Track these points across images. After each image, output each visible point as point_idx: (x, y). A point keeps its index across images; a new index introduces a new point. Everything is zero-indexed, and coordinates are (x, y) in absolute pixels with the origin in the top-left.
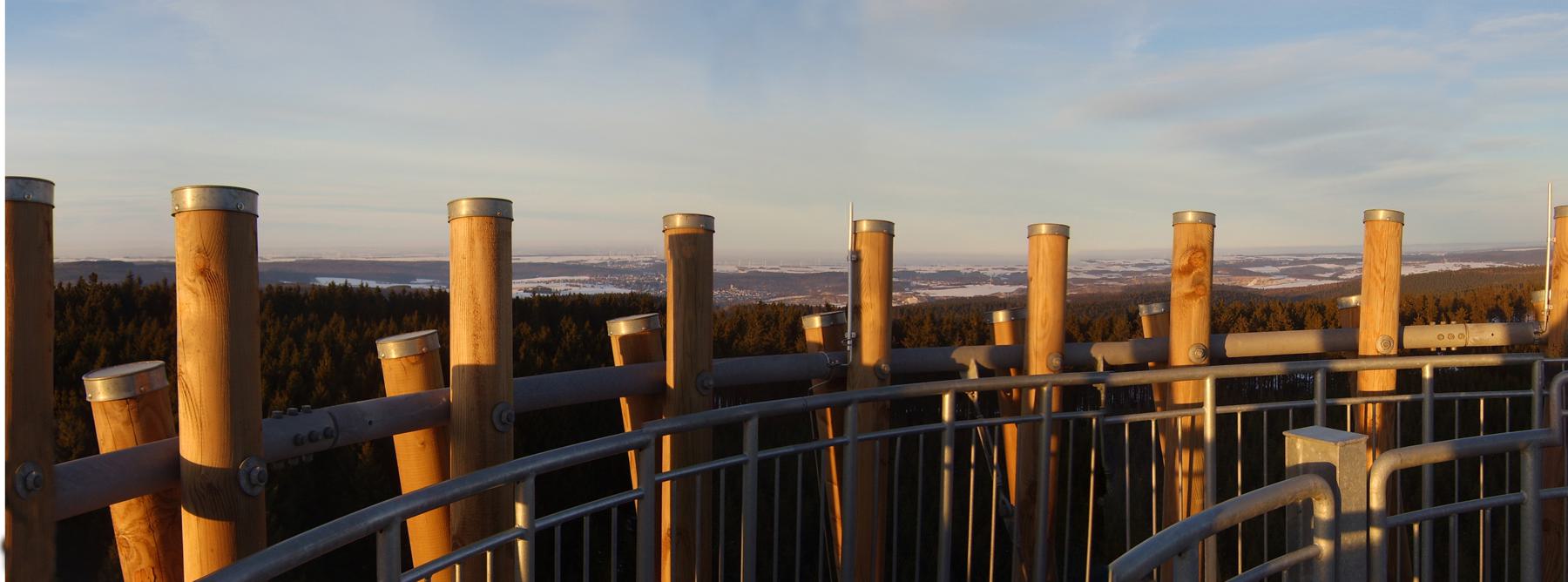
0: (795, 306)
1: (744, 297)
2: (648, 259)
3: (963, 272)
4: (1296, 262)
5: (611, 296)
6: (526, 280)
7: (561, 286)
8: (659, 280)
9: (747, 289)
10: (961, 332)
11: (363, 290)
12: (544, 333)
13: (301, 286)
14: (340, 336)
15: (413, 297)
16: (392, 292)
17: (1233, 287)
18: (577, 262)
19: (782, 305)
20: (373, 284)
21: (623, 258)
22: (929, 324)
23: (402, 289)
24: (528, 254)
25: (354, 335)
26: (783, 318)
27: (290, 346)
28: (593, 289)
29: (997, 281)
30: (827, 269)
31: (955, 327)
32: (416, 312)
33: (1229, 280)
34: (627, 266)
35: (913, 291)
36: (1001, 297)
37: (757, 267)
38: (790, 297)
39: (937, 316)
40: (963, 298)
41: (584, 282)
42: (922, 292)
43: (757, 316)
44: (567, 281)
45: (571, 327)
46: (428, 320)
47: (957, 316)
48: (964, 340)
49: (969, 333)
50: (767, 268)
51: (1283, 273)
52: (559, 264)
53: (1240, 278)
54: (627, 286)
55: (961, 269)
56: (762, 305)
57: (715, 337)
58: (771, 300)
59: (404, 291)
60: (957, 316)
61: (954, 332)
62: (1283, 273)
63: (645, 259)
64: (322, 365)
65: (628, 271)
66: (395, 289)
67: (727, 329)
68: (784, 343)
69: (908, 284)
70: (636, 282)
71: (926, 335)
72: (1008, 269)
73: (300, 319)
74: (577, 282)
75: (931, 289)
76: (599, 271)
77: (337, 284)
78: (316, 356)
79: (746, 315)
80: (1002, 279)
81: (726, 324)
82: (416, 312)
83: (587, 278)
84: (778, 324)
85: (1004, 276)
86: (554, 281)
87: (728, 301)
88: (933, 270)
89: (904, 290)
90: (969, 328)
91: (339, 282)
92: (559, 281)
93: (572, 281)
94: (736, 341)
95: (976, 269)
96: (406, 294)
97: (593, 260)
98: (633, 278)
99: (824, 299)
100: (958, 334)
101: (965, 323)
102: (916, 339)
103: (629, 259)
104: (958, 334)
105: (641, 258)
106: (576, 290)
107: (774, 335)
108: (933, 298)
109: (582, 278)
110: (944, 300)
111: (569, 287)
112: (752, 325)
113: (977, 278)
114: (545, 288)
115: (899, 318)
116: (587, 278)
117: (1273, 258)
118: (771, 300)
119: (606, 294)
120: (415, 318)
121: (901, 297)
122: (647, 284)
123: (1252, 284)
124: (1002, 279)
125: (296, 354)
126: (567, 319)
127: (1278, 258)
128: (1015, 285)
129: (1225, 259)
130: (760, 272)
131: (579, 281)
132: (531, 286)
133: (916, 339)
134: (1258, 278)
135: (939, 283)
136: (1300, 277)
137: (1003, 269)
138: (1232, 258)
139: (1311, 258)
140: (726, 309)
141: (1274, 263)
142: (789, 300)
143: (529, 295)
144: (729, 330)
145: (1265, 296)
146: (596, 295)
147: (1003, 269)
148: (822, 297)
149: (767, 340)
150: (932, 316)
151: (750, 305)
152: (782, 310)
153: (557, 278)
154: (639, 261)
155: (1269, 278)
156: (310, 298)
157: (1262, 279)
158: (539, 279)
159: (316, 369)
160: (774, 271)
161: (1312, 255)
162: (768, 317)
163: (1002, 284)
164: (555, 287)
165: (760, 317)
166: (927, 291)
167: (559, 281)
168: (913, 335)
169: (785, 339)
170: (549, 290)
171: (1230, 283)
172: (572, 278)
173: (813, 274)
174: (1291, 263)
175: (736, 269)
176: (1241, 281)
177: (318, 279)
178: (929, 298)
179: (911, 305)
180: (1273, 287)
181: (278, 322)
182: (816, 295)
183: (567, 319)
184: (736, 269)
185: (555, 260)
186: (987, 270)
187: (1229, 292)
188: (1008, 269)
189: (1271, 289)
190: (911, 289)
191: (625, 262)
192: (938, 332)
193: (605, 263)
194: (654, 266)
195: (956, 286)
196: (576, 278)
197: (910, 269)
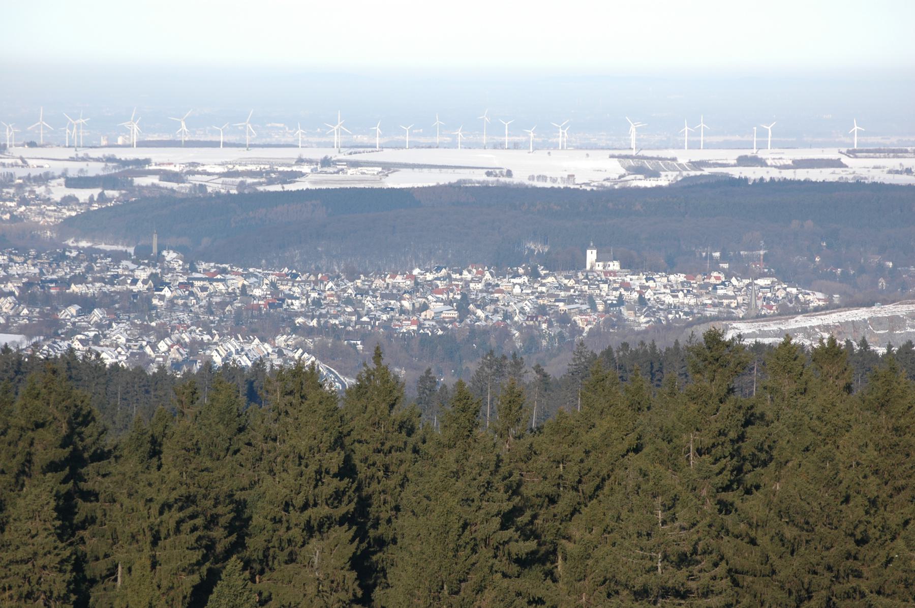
2: (95, 169)
63: (74, 169)
122: (87, 304)
130: (743, 181)
154: (44, 179)
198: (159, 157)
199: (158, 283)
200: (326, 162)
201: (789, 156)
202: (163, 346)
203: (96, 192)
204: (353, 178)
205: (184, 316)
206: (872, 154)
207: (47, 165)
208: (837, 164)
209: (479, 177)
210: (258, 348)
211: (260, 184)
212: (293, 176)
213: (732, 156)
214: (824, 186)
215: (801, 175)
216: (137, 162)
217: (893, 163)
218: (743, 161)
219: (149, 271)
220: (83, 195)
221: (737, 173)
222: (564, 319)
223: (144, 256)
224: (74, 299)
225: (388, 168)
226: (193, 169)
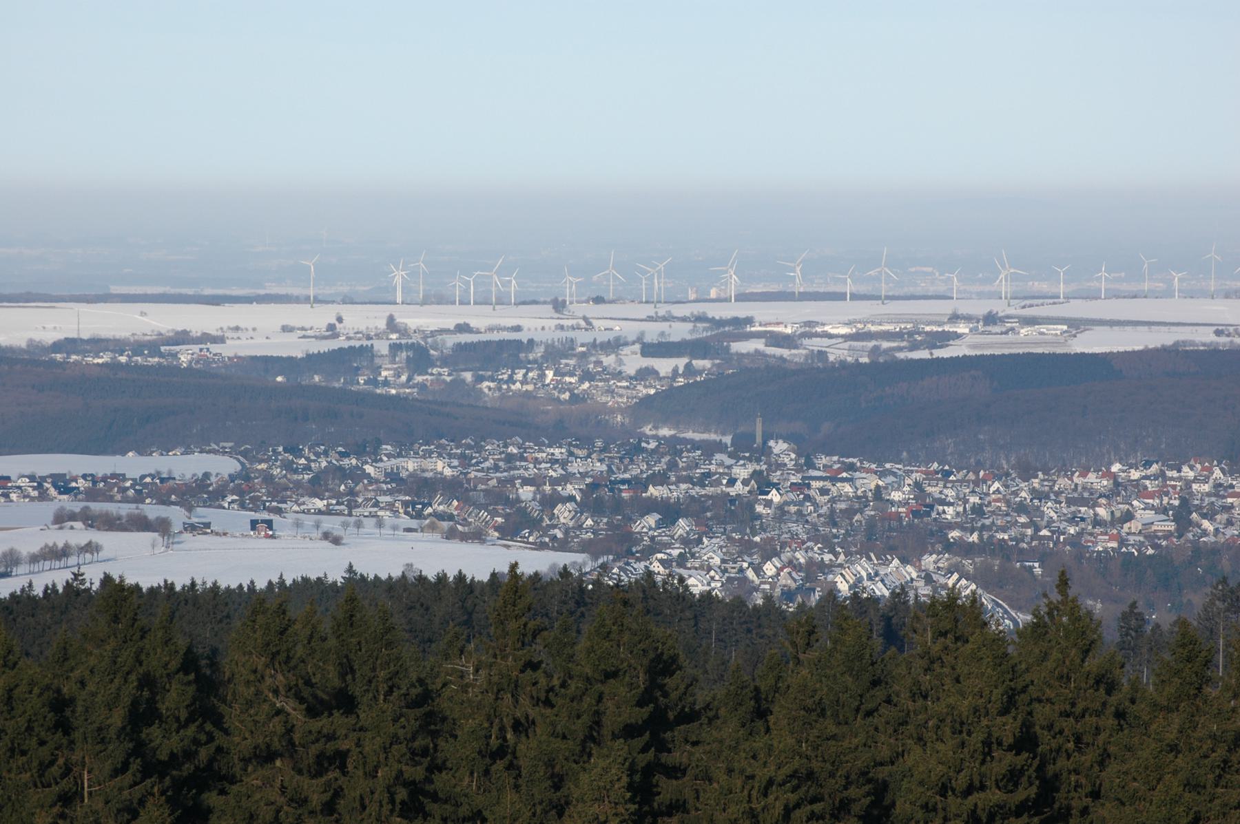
2: (680, 332)
28: (259, 544)
34: (520, 382)
44: (63, 484)
63: (653, 332)
83: (222, 466)
93: (100, 488)
111: (78, 535)
116: (222, 466)
122: (669, 513)
154: (614, 346)
196: (133, 465)
199: (763, 484)
200: (990, 319)
202: (769, 569)
203: (681, 362)
204: (1026, 340)
209: (1206, 337)
210: (899, 572)
211: (900, 349)
212: (944, 338)
216: (736, 322)
219: (751, 467)
220: (664, 366)
223: (745, 448)
225: (1077, 325)
226: (809, 330)
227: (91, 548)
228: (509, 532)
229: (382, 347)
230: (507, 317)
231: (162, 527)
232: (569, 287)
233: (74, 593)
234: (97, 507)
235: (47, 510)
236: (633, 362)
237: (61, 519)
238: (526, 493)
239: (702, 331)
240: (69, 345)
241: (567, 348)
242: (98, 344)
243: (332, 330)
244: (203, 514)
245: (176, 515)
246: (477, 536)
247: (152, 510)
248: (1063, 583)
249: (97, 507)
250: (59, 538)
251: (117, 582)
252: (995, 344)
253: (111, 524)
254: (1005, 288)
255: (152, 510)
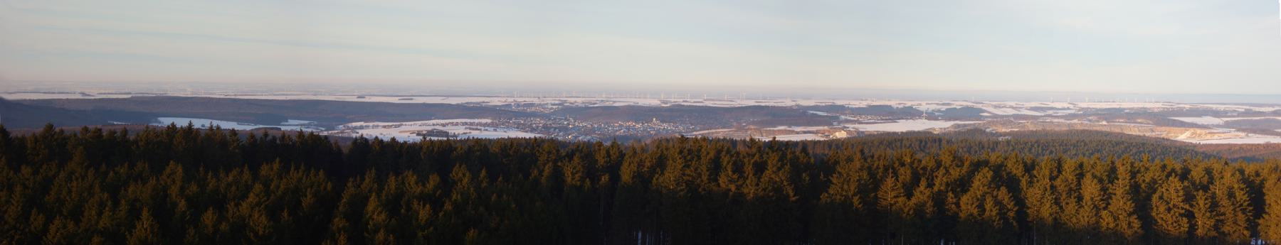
0: (719, 139)
1: (667, 131)
2: (557, 102)
3: (895, 106)
4: (1247, 113)
5: (512, 141)
6: (420, 122)
7: (459, 130)
8: (568, 124)
9: (670, 122)
10: (893, 168)
11: (213, 133)
12: (434, 180)
13: (128, 129)
14: (174, 191)
15: (278, 142)
16: (252, 135)
17: (1156, 139)
18: (478, 103)
19: (704, 139)
20: (226, 125)
21: (529, 100)
22: (859, 160)
23: (263, 131)
24: (422, 94)
25: (194, 188)
26: (705, 153)
27: (102, 205)
28: (495, 133)
29: (931, 116)
30: (751, 103)
31: (886, 163)
32: (278, 160)
33: (1153, 131)
34: (533, 109)
35: (842, 125)
36: (935, 133)
37: (680, 101)
38: (714, 131)
39: (866, 151)
40: (894, 133)
41: (485, 125)
42: (851, 127)
43: (678, 150)
44: (466, 124)
45: (464, 175)
46: (292, 169)
47: (889, 151)
48: (897, 177)
49: (902, 170)
50: (691, 102)
51: (1227, 125)
52: (458, 105)
53: (1168, 128)
54: (533, 130)
55: (894, 103)
56: (683, 140)
57: (635, 172)
58: (695, 133)
59: (266, 135)
60: (889, 151)
61: (886, 169)
62: (1227, 125)
63: (553, 102)
64: (139, 227)
65: (534, 115)
66: (255, 133)
67: (648, 164)
68: (706, 178)
69: (836, 119)
70: (543, 127)
71: (856, 172)
72: (943, 104)
73: (123, 170)
74: (477, 124)
75: (860, 123)
76: (501, 114)
77: (178, 126)
78: (135, 214)
79: (667, 149)
80: (936, 114)
81: (646, 158)
82: (278, 160)
83: (489, 121)
84: (700, 159)
85: (939, 111)
86: (452, 124)
87: (651, 134)
88: (863, 104)
89: (831, 124)
90: (903, 165)
91: (182, 123)
92: (457, 124)
93: (471, 124)
94: (657, 176)
95: (909, 104)
96: (269, 138)
97: (496, 102)
98: (540, 122)
99: (749, 132)
100: (891, 171)
101: (898, 160)
102: (845, 175)
103: (536, 101)
104: (891, 171)
105: (549, 101)
106: (476, 134)
107: (696, 169)
108: (863, 132)
109: (484, 121)
110: (874, 135)
111: (468, 131)
112: (673, 160)
113: (910, 113)
114: (441, 131)
115: (826, 152)
116: (489, 121)
117: (1214, 107)
118: (695, 133)
119: (509, 138)
120: (276, 166)
121: (829, 131)
122: (555, 128)
123: (1184, 137)
124: (936, 114)
125: (107, 213)
126: (460, 166)
127: (1222, 108)
128: (950, 120)
129: (1148, 105)
130: (684, 106)
131: (480, 124)
132: (425, 129)
133: (845, 175)
134: (1192, 130)
135: (869, 117)
136: (1255, 132)
137: (937, 104)
138: (1159, 105)
139: (1271, 109)
140: (648, 142)
141: (1216, 114)
142: (713, 133)
143: (419, 139)
144: (649, 164)
145: (1203, 153)
146: (498, 139)
147: (937, 104)
148: (747, 130)
149: (689, 175)
150: (862, 151)
151: (672, 139)
152: (704, 144)
153: (455, 121)
154: (547, 104)
155: (1207, 131)
156: (140, 144)
157: (1199, 131)
158: (434, 121)
159: (130, 233)
160: (698, 104)
161: (1272, 106)
162: (690, 151)
163: (936, 119)
164: (452, 130)
165: (681, 152)
166: (857, 126)
167: (457, 124)
168: (843, 171)
169: (708, 173)
170: (446, 134)
171: (1153, 135)
172: (472, 121)
173: (739, 108)
174: (1240, 114)
175: (659, 102)
176: (1169, 132)
177: (161, 119)
178: (858, 132)
179: (839, 140)
180: (1214, 142)
181: (91, 172)
182: (740, 129)
183: (460, 166)
184: (659, 102)
185: (454, 101)
186: (920, 105)
187: (1153, 145)
188: (943, 104)
189: (1211, 145)
190: (840, 122)
191: (532, 105)
192: (869, 168)
193: (509, 105)
194: (562, 109)
195: (886, 121)
196: (476, 121)
197: (839, 103)
198: (569, 99)
199: (568, 124)
200: (602, 101)
201: (693, 100)
204: (607, 104)
205: (27, 230)
206: (1257, 109)
207: (548, 102)
208: (701, 102)
209: (632, 104)
210: (589, 137)
212: (596, 103)
213: (681, 100)
214: (699, 107)
215: (695, 104)
217: (712, 102)
218: (684, 101)
220: (554, 107)
221: (683, 104)
222: (649, 132)
223: (566, 120)
224: (553, 127)
225: (614, 102)
226: (576, 102)
227: (470, 133)
228: (531, 131)
229: (513, 104)
230: (531, 99)
231: (480, 130)
232: (541, 96)
233: (468, 139)
234: (472, 127)
235: (464, 127)
236: (550, 107)
237: (466, 128)
238: (534, 125)
239: (560, 102)
240: (467, 103)
241: (540, 104)
242: (471, 103)
243: (505, 101)
244: (486, 128)
245: (483, 128)
246: (527, 132)
247: (479, 127)
248: (615, 139)
249: (472, 127)
250: (465, 131)
251: (1028, 220)
252: (602, 105)
253: (473, 129)
254: (604, 96)
255: (479, 127)
